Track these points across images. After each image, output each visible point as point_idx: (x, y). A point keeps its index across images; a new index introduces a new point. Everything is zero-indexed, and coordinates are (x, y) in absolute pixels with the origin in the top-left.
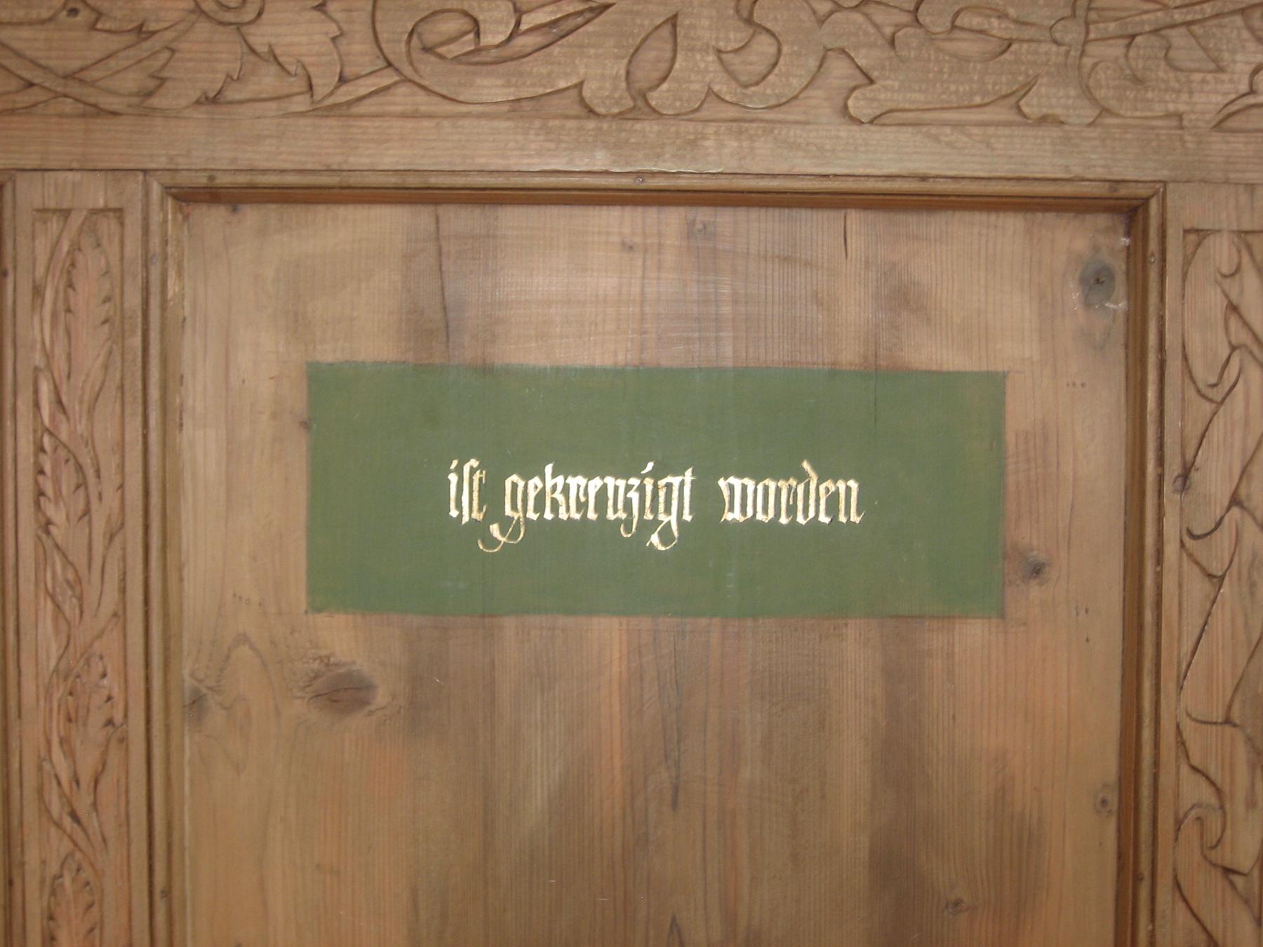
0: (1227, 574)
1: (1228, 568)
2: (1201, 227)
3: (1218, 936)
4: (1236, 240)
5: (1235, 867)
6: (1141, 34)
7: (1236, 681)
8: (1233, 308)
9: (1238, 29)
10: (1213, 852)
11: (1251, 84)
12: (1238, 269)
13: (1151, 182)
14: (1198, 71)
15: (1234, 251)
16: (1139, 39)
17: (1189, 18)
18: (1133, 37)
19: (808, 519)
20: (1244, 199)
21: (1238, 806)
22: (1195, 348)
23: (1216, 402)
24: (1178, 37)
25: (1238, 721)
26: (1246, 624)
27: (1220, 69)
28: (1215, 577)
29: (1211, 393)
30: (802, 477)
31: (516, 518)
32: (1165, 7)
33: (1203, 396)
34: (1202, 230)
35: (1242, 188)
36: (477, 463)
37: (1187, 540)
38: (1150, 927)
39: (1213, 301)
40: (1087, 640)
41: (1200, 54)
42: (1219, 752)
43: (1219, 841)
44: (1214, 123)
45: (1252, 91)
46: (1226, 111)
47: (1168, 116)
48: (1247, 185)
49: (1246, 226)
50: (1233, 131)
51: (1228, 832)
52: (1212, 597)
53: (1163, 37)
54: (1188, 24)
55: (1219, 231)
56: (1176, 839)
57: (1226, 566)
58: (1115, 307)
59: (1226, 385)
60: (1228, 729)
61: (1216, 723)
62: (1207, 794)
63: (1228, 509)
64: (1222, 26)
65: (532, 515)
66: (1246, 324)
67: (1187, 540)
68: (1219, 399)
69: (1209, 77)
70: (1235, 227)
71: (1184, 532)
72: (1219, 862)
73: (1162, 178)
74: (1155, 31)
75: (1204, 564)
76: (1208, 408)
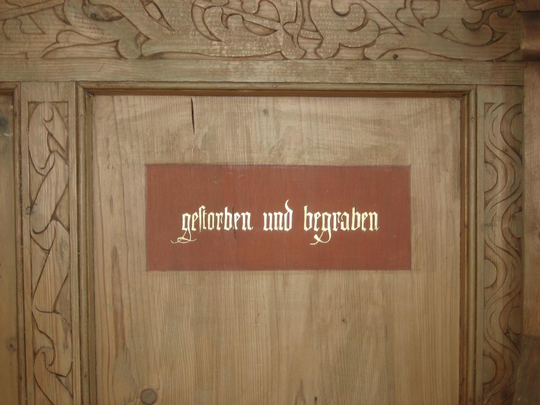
0: (51, 249)
1: (52, 246)
2: (35, 101)
3: (55, 402)
4: (51, 106)
5: (60, 374)
6: (9, 19)
7: (57, 295)
8: (50, 135)
9: (50, 15)
10: (50, 367)
11: (57, 39)
12: (52, 118)
13: (15, 82)
14: (34, 34)
15: (50, 110)
16: (8, 22)
17: (29, 11)
18: (5, 20)
19: (357, 228)
20: (54, 88)
21: (60, 347)
22: (34, 153)
23: (44, 176)
24: (26, 20)
25: (59, 312)
26: (60, 270)
27: (44, 33)
28: (46, 250)
29: (43, 172)
30: (284, 211)
31: (186, 230)
32: (19, 7)
33: (38, 173)
34: (37, 102)
35: (53, 84)
36: (205, 207)
37: (32, 234)
38: (26, 399)
39: (41, 132)
40: (1, 277)
41: (34, 26)
42: (51, 324)
43: (52, 363)
44: (41, 56)
45: (58, 42)
46: (46, 51)
47: (21, 53)
48: (55, 82)
49: (56, 100)
50: (50, 59)
51: (56, 359)
52: (45, 258)
53: (19, 20)
54: (29, 14)
55: (44, 102)
56: (34, 362)
57: (50, 245)
58: (8, 135)
59: (48, 169)
60: (54, 314)
61: (49, 312)
62: (48, 344)
63: (51, 221)
64: (44, 14)
65: (194, 229)
66: (57, 142)
67: (32, 234)
68: (45, 174)
69: (38, 36)
70: (50, 100)
71: (31, 230)
72: (53, 371)
73: (19, 80)
74: (16, 18)
75: (41, 244)
76: (41, 178)
